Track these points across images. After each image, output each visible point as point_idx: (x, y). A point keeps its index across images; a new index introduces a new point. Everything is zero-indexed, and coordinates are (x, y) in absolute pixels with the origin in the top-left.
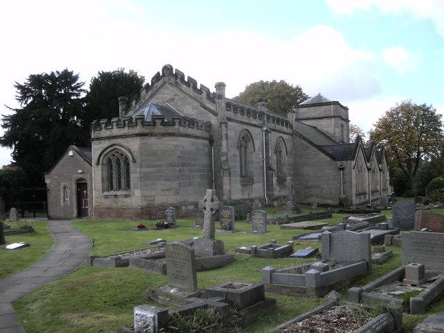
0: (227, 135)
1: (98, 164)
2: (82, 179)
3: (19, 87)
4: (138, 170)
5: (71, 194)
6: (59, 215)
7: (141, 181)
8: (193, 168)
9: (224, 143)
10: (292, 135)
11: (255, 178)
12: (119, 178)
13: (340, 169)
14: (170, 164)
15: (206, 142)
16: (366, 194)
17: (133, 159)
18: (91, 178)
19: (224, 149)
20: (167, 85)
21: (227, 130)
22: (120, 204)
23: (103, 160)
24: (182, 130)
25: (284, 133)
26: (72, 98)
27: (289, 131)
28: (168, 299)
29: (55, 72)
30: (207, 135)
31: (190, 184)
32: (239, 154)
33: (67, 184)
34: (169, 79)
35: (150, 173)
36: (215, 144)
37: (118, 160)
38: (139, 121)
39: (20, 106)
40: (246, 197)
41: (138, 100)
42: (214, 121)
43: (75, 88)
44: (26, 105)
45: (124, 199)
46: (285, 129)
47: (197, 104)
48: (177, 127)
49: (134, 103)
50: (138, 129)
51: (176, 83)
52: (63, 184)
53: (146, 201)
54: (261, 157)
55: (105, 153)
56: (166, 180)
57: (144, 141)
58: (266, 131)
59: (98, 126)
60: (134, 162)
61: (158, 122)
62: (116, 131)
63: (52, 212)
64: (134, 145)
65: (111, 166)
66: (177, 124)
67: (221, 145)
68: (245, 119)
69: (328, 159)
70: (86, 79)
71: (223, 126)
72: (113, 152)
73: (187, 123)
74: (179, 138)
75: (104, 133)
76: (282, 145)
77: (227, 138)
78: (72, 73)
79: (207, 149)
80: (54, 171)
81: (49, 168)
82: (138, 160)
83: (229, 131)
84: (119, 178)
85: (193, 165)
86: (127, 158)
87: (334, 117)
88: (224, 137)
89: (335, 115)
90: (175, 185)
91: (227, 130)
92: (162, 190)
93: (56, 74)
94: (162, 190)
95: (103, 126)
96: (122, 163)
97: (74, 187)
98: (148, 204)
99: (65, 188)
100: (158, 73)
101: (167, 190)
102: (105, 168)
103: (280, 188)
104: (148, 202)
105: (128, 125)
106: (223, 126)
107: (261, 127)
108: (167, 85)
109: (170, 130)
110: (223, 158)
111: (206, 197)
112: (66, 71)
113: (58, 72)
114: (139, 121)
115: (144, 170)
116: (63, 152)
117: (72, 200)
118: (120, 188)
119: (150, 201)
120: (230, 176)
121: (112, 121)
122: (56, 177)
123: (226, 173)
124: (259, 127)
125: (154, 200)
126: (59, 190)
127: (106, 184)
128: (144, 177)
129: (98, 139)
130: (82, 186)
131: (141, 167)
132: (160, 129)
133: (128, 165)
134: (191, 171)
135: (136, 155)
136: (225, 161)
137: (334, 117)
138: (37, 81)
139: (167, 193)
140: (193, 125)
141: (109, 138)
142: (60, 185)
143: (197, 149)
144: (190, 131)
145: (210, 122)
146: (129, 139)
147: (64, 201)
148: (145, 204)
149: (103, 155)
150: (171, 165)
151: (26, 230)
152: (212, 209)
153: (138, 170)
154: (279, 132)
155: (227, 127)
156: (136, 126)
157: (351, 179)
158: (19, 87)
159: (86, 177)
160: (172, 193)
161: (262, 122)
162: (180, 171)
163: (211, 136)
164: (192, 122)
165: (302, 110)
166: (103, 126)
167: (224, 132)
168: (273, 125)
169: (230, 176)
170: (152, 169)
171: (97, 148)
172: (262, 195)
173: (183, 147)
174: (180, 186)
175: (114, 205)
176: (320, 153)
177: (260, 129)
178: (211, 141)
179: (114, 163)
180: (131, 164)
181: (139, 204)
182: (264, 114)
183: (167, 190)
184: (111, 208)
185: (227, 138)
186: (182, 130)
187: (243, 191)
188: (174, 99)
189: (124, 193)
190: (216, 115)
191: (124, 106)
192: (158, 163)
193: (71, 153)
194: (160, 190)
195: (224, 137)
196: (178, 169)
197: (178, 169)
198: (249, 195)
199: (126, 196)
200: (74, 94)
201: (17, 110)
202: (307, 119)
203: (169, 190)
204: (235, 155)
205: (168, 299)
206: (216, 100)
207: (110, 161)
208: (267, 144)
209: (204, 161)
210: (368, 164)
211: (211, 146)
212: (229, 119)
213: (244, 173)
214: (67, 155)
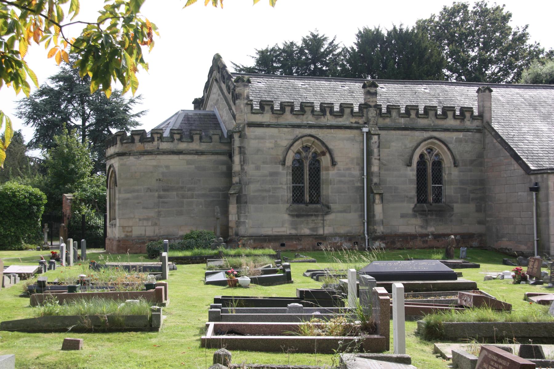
10: (479, 131)
13: (532, 189)
14: (148, 189)
28: (11, 345)
29: (305, 38)
31: (180, 213)
35: (128, 199)
48: (155, 143)
54: (357, 172)
56: (144, 208)
66: (156, 139)
70: (385, 33)
74: (159, 157)
90: (152, 213)
92: (140, 220)
94: (140, 220)
98: (127, 236)
100: (433, 16)
101: (144, 219)
104: (125, 233)
107: (359, 128)
109: (148, 147)
119: (127, 232)
125: (131, 231)
136: (237, 183)
139: (145, 223)
148: (123, 235)
150: (149, 190)
151: (426, 245)
160: (150, 224)
162: (160, 197)
172: (362, 231)
176: (513, 162)
177: (356, 132)
183: (144, 219)
192: (136, 188)
194: (138, 220)
203: (147, 219)
205: (11, 345)
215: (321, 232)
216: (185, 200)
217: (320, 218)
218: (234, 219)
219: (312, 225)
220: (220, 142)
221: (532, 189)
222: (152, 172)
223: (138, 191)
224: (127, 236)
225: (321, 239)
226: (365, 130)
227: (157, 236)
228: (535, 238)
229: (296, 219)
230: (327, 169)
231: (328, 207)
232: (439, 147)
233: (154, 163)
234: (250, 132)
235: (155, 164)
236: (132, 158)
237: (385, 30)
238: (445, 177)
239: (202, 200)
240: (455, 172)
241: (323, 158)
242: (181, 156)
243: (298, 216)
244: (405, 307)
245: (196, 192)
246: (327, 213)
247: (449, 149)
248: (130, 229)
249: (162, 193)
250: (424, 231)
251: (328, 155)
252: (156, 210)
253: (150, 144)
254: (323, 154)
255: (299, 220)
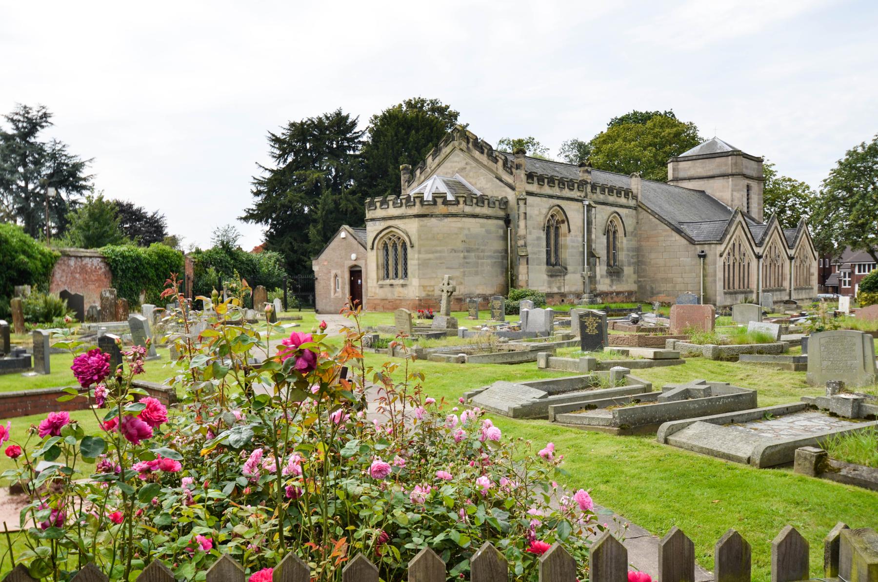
0: (525, 213)
1: (372, 248)
2: (356, 266)
3: (276, 140)
4: (416, 256)
5: (343, 283)
6: (328, 308)
7: (419, 269)
8: (482, 254)
9: (522, 223)
10: (635, 209)
11: (569, 268)
12: (396, 264)
13: (700, 256)
15: (501, 223)
16: (752, 292)
17: (411, 243)
18: (366, 264)
19: (522, 231)
20: (457, 152)
21: (526, 208)
22: (396, 295)
23: (378, 244)
24: (468, 209)
25: (621, 206)
26: (348, 152)
27: (632, 203)
30: (502, 213)
31: (476, 273)
32: (545, 237)
33: (339, 272)
34: (460, 144)
35: (429, 259)
36: (511, 225)
37: (395, 246)
38: (417, 201)
39: (274, 165)
40: (555, 290)
41: (423, 170)
42: (511, 196)
43: (352, 140)
44: (285, 166)
45: (401, 289)
46: (623, 200)
47: (491, 176)
48: (461, 206)
49: (418, 172)
50: (417, 209)
51: (468, 148)
52: (333, 272)
53: (425, 291)
54: (580, 239)
55: (381, 235)
56: (447, 268)
57: (421, 223)
58: (589, 206)
59: (372, 204)
60: (412, 247)
61: (439, 201)
62: (392, 211)
63: (320, 303)
64: (411, 227)
65: (387, 251)
66: (461, 202)
67: (518, 226)
68: (556, 191)
69: (684, 242)
71: (521, 203)
72: (389, 235)
73: (475, 201)
74: (464, 219)
75: (379, 213)
76: (618, 223)
77: (525, 218)
78: (347, 117)
79: (501, 232)
80: (323, 256)
81: (318, 253)
82: (416, 244)
83: (528, 208)
84: (396, 264)
85: (483, 251)
86: (404, 244)
87: (733, 175)
88: (522, 216)
89: (734, 171)
91: (526, 208)
93: (324, 120)
95: (378, 204)
96: (399, 248)
97: (347, 276)
99: (336, 276)
102: (381, 253)
103: (612, 281)
104: (426, 292)
105: (406, 204)
106: (521, 203)
107: (581, 201)
108: (457, 152)
109: (453, 209)
110: (521, 242)
111: (444, 282)
112: (338, 114)
113: (327, 118)
114: (417, 201)
115: (424, 256)
116: (335, 231)
117: (343, 292)
118: (397, 277)
120: (527, 263)
121: (388, 199)
122: (326, 264)
123: (523, 261)
124: (577, 200)
125: (433, 291)
126: (329, 280)
127: (382, 273)
128: (423, 264)
129: (372, 220)
130: (355, 274)
131: (419, 252)
132: (441, 208)
133: (405, 250)
134: (478, 258)
135: (414, 239)
136: (522, 246)
137: (733, 175)
138: (300, 131)
140: (483, 203)
141: (384, 219)
142: (330, 272)
143: (488, 232)
144: (478, 210)
145: (506, 198)
146: (406, 220)
147: (335, 292)
148: (423, 294)
149: (378, 238)
152: (448, 292)
153: (416, 256)
154: (612, 205)
155: (525, 204)
156: (414, 205)
157: (715, 271)
158: (276, 140)
159: (361, 263)
161: (583, 194)
162: (465, 258)
163: (508, 216)
164: (481, 200)
165: (682, 165)
166: (378, 204)
167: (522, 210)
168: (602, 196)
169: (527, 263)
170: (431, 256)
171: (372, 229)
173: (469, 229)
174: (464, 275)
175: (390, 296)
176: (674, 234)
177: (580, 204)
178: (507, 221)
179: (390, 248)
180: (409, 249)
181: (417, 295)
182: (587, 183)
184: (386, 299)
185: (525, 218)
186: (468, 209)
187: (550, 284)
188: (465, 168)
189: (401, 282)
190: (513, 189)
191: (407, 176)
192: (439, 248)
193: (343, 234)
195: (522, 216)
196: (462, 255)
197: (462, 255)
198: (559, 288)
199: (403, 286)
200: (349, 148)
201: (272, 171)
202: (690, 179)
204: (539, 239)
206: (514, 170)
207: (386, 244)
208: (589, 223)
209: (498, 245)
210: (791, 252)
211: (507, 227)
212: (529, 194)
213: (553, 260)
214: (338, 236)
215: (562, 291)
216: (480, 261)
217: (562, 278)
218: (524, 278)
219: (558, 284)
220: (500, 208)
221: (700, 256)
222: (456, 234)
223: (440, 252)
224: (428, 295)
225: (563, 295)
226: (587, 203)
227: (462, 294)
228: (702, 294)
229: (550, 279)
230: (565, 236)
231: (566, 269)
232: (617, 220)
233: (459, 225)
234: (530, 199)
235: (460, 226)
236: (433, 220)
237: (644, 112)
238: (618, 245)
239: (489, 261)
240: (625, 240)
241: (562, 225)
242: (477, 220)
243: (551, 276)
244: (807, 353)
245: (486, 254)
246: (566, 274)
247: (623, 222)
248: (432, 289)
249: (466, 254)
250: (611, 289)
251: (566, 223)
252: (462, 270)
253: (455, 206)
254: (563, 222)
255: (553, 279)
